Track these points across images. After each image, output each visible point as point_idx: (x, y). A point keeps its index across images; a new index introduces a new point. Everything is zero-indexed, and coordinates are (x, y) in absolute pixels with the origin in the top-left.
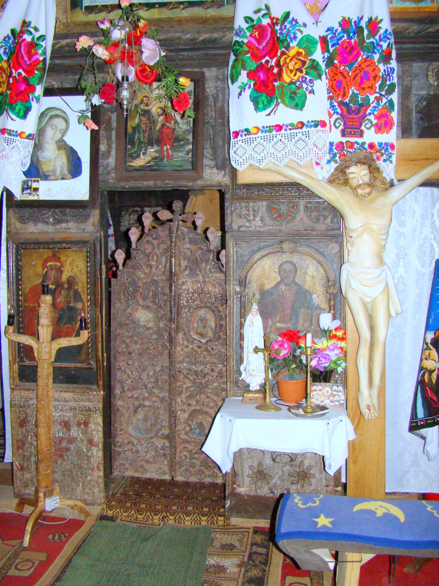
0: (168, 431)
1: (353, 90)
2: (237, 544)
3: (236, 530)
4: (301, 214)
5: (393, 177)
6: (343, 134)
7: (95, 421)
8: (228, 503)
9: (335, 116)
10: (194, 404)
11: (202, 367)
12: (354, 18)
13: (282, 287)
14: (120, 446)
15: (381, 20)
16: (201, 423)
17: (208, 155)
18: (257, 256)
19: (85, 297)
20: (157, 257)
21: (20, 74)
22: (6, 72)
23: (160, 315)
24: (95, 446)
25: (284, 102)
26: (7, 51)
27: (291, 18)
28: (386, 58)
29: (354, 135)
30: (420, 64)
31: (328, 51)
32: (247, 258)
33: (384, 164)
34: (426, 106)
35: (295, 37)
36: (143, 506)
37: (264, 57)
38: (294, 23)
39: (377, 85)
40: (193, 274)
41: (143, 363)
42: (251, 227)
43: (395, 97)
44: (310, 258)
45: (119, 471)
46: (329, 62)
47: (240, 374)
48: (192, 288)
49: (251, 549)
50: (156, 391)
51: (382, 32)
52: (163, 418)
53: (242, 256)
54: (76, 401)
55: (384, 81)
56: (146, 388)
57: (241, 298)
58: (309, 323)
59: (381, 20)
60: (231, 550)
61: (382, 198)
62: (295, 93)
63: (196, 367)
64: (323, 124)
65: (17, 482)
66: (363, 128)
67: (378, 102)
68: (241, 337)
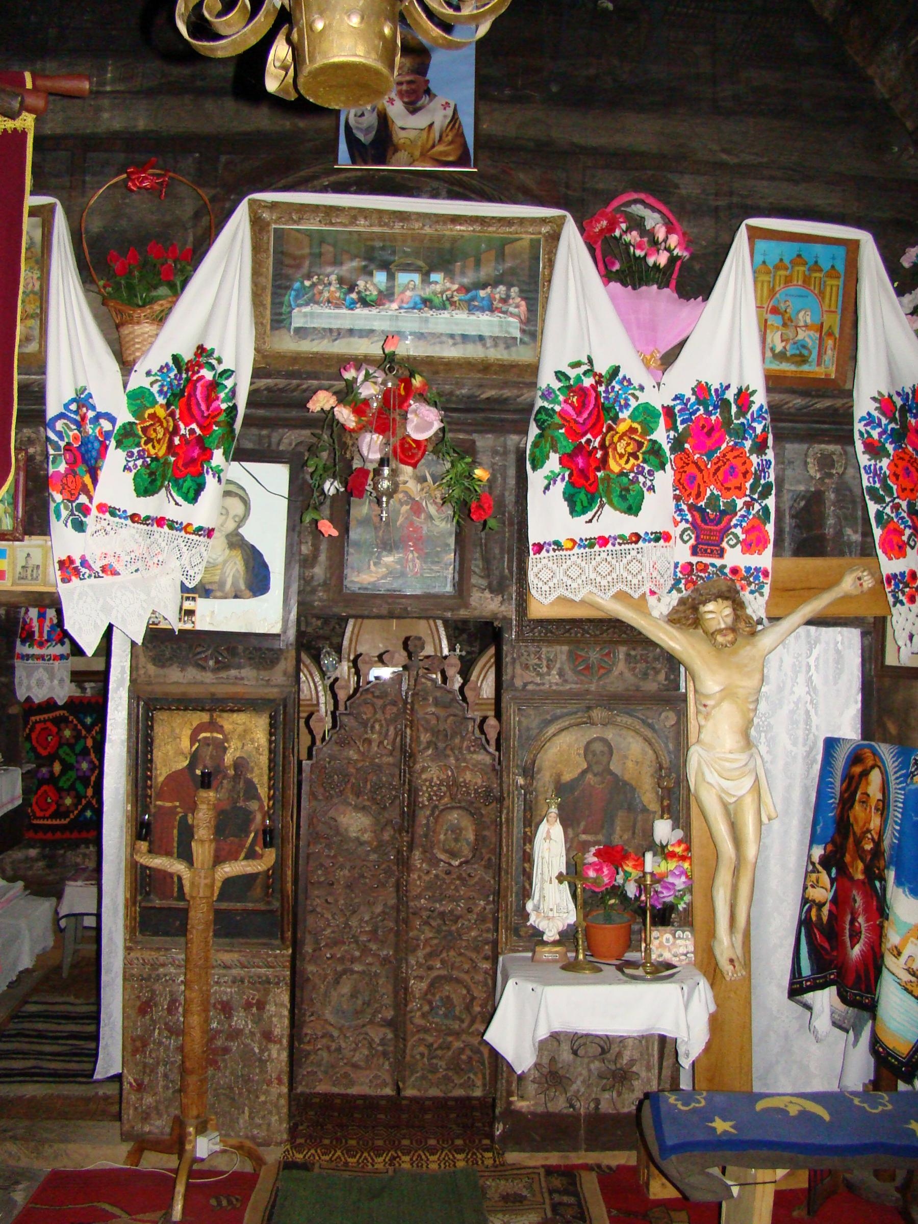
0: (392, 1013)
1: (711, 490)
2: (525, 1193)
3: (517, 1171)
4: (621, 666)
5: (764, 616)
6: (694, 551)
7: (277, 1000)
8: (499, 1129)
9: (683, 525)
10: (438, 966)
12: (715, 386)
13: (589, 776)
14: (309, 1042)
15: (754, 392)
16: (448, 997)
17: (477, 570)
18: (552, 730)
19: (263, 791)
20: (381, 726)
21: (192, 431)
22: (165, 425)
23: (383, 821)
24: (275, 1042)
25: (611, 504)
26: (165, 389)
27: (620, 376)
28: (760, 447)
29: (711, 554)
30: (796, 446)
31: (675, 429)
32: (536, 731)
33: (751, 597)
34: (802, 509)
35: (627, 405)
36: (353, 1142)
37: (585, 434)
38: (625, 383)
39: (748, 485)
40: (440, 755)
41: (352, 899)
42: (543, 684)
43: (771, 502)
44: (633, 734)
45: (307, 1085)
46: (677, 445)
47: (527, 916)
49: (551, 1199)
50: (374, 947)
51: (754, 408)
52: (384, 991)
54: (243, 966)
55: (757, 479)
56: (357, 942)
57: (525, 795)
58: (630, 833)
59: (754, 392)
60: (521, 1202)
61: (748, 648)
62: (627, 490)
63: (441, 905)
64: (667, 537)
65: (129, 1114)
66: (724, 545)
67: (748, 509)
68: (528, 858)
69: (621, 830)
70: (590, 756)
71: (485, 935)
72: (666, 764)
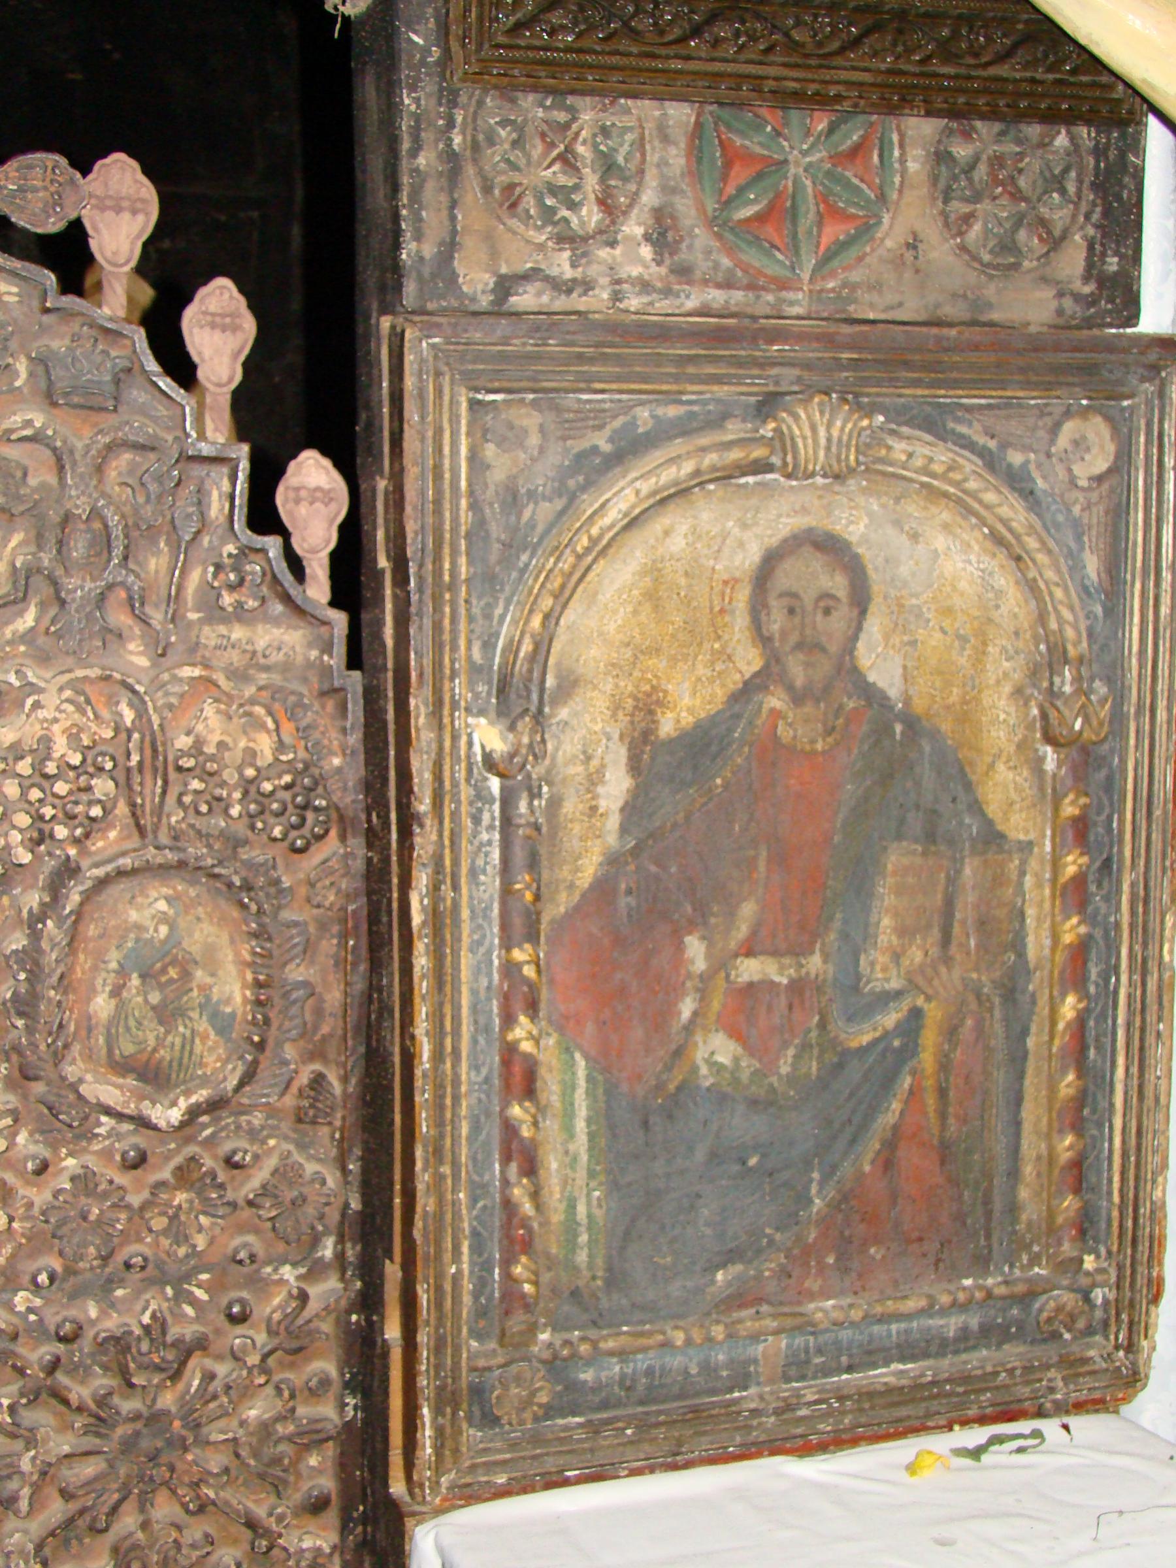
4: (910, 214)
11: (154, 1303)
18: (622, 496)
42: (587, 286)
48: (73, 738)
53: (512, 498)
57: (508, 801)
69: (902, 931)
70: (776, 622)
71: (303, 1411)
72: (1077, 645)
